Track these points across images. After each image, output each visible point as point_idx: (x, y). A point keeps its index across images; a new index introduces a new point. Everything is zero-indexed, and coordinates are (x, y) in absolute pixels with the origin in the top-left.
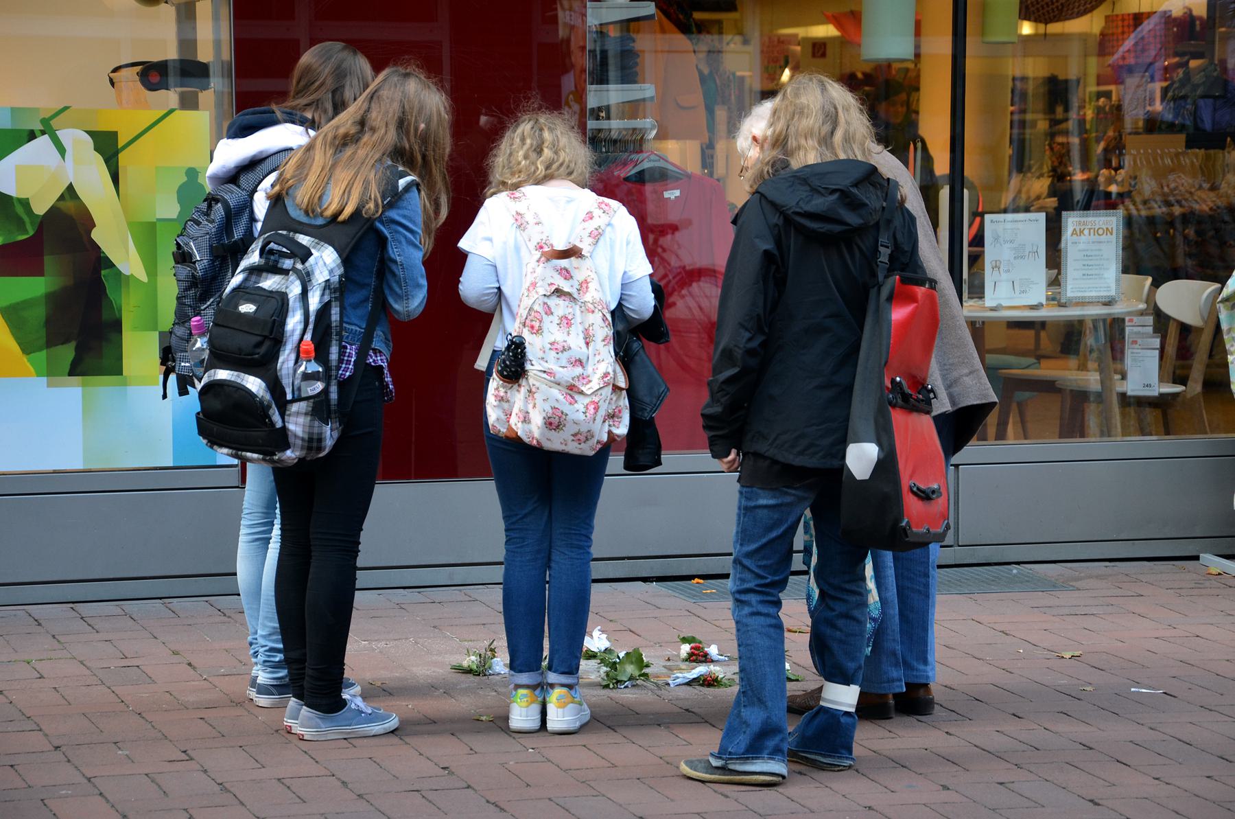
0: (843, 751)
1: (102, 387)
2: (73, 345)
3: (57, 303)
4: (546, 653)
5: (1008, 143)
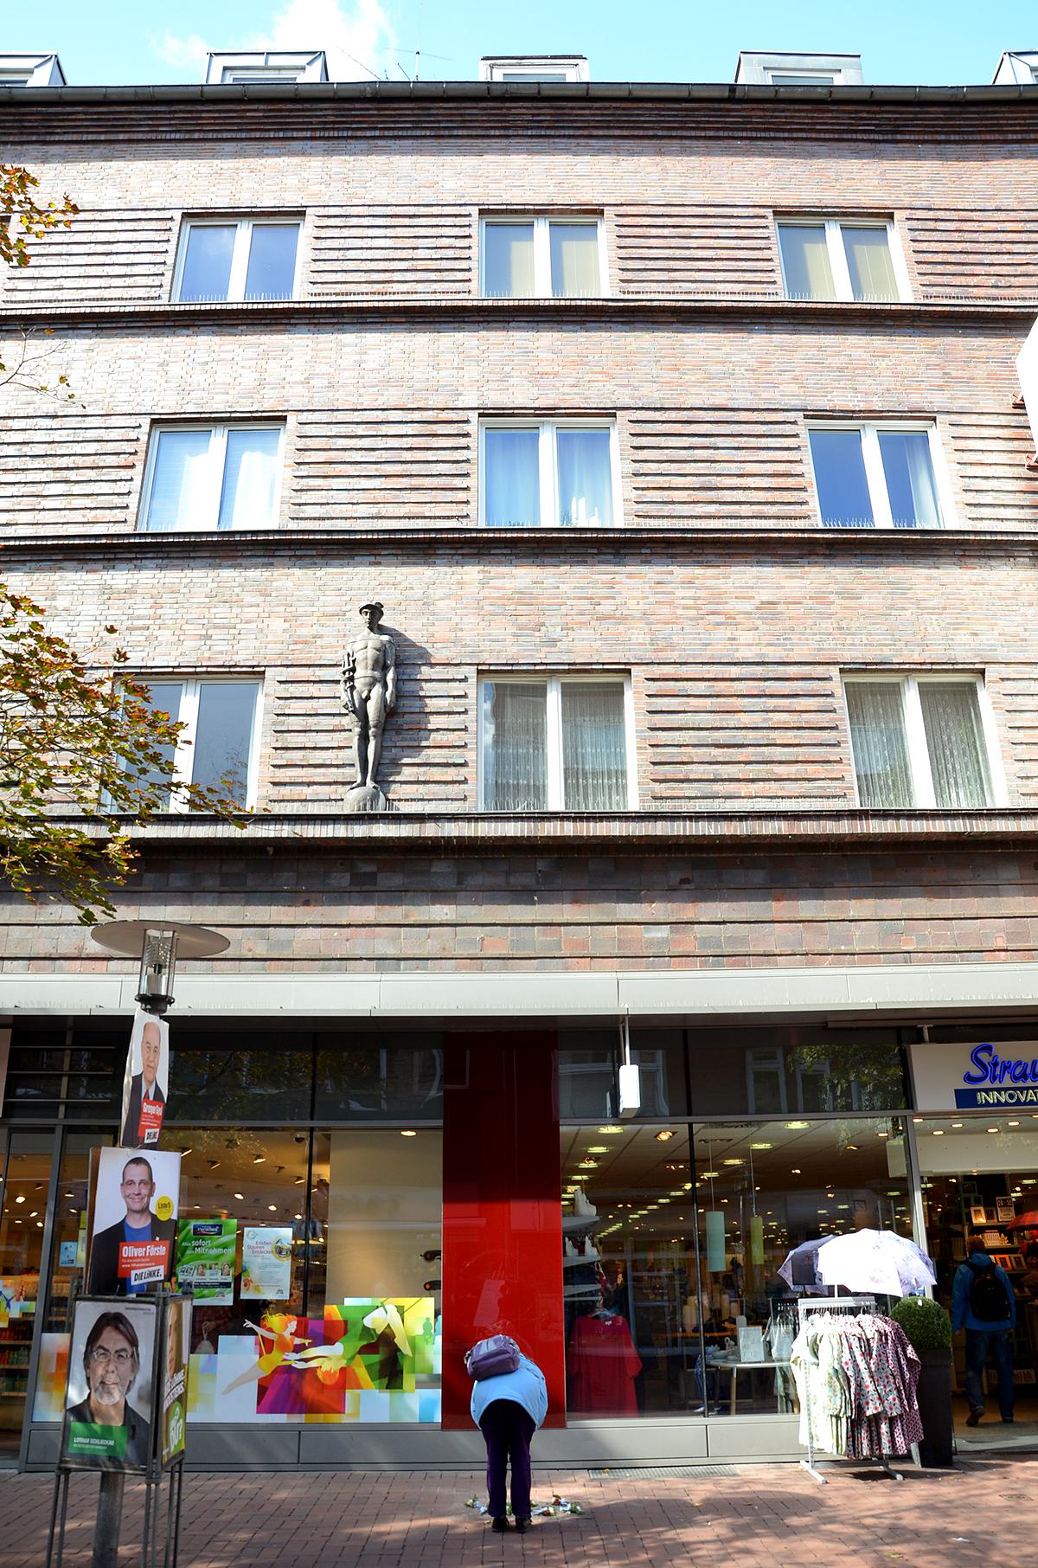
0: (1009, 1514)
1: (396, 1393)
2: (387, 1379)
3: (383, 1364)
4: (509, 1500)
5: (787, 199)
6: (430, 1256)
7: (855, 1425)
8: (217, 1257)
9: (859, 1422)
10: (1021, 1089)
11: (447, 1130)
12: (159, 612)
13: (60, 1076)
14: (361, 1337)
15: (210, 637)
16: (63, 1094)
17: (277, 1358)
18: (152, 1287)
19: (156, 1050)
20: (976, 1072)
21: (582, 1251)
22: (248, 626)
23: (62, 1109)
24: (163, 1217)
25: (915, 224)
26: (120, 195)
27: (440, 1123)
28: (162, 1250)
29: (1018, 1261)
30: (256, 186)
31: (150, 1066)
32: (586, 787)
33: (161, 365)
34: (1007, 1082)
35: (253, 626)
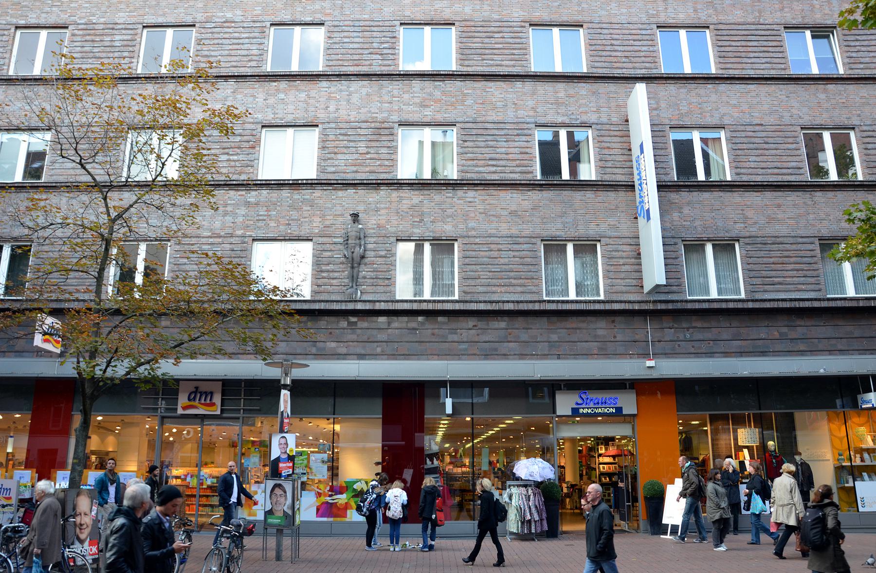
6: (377, 464)
7: (523, 523)
8: (301, 464)
9: (524, 522)
10: (596, 408)
11: (383, 419)
12: (270, 213)
13: (240, 399)
14: (353, 492)
15: (290, 225)
16: (242, 405)
17: (323, 499)
18: (289, 475)
19: (287, 401)
20: (580, 401)
21: (433, 463)
22: (305, 220)
23: (242, 411)
24: (291, 454)
25: (593, 31)
26: (242, 14)
27: (381, 416)
28: (291, 464)
29: (615, 468)
30: (302, 10)
31: (286, 407)
32: (439, 285)
33: (264, 100)
34: (592, 405)
35: (307, 220)
